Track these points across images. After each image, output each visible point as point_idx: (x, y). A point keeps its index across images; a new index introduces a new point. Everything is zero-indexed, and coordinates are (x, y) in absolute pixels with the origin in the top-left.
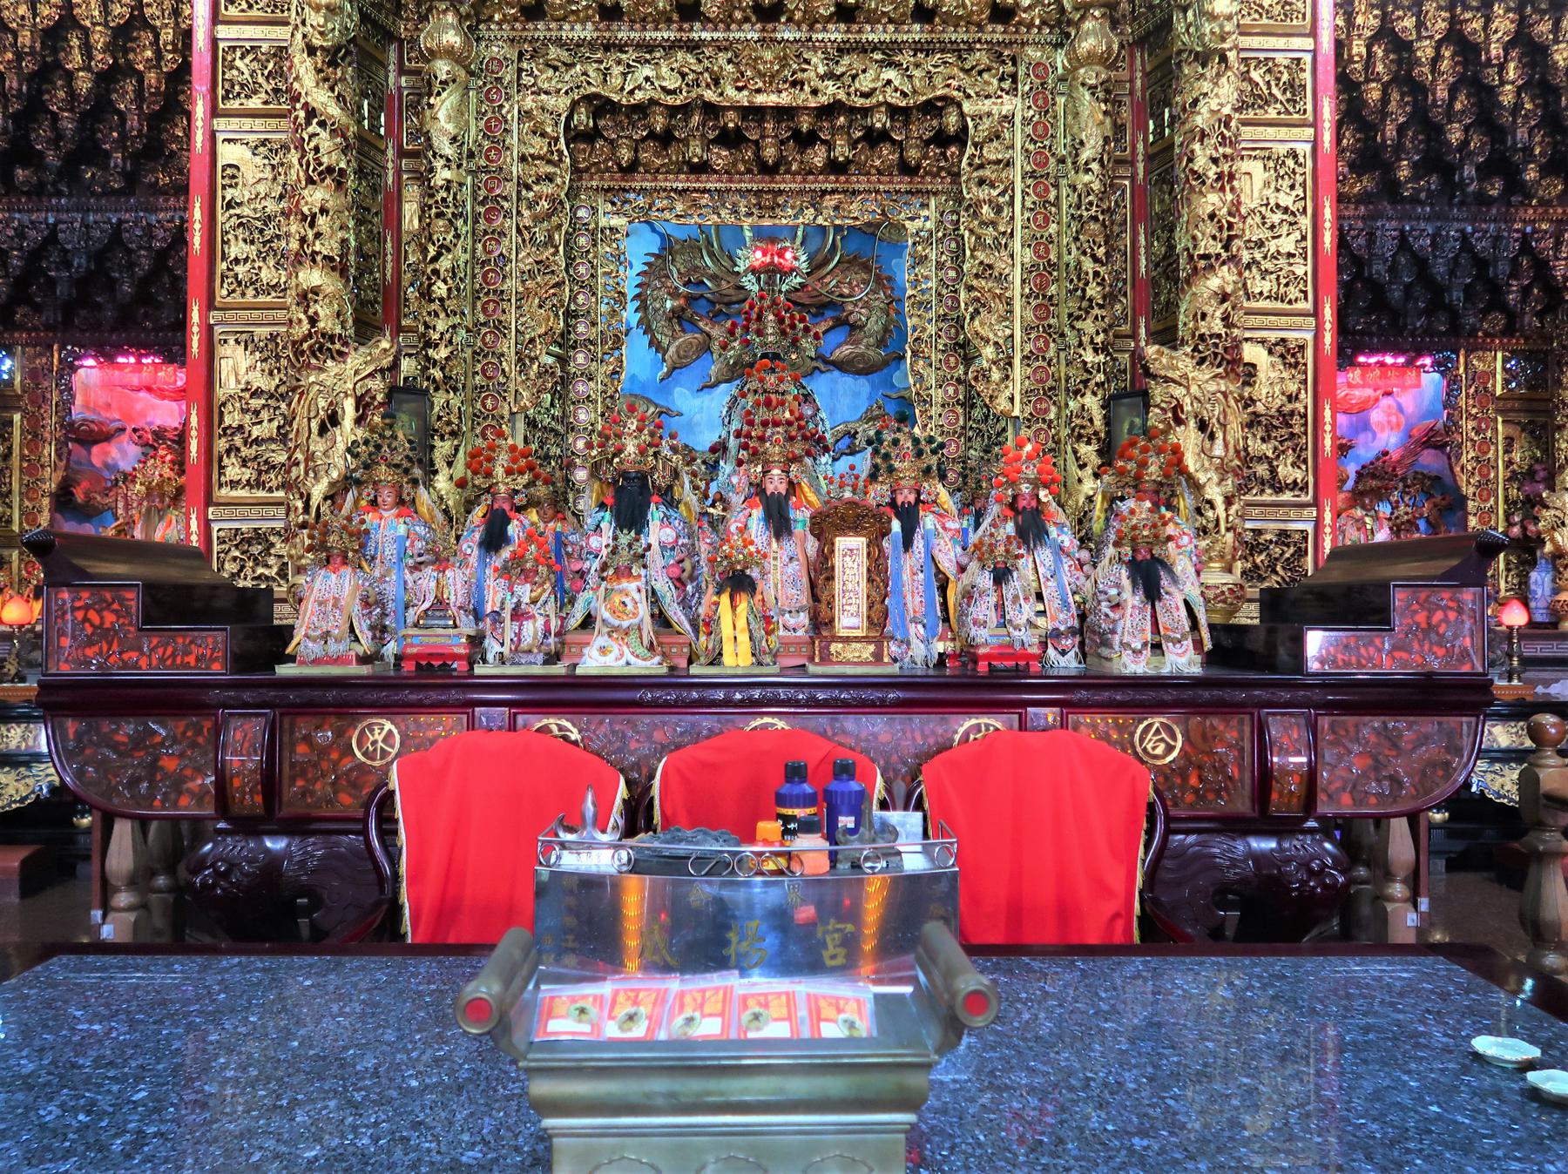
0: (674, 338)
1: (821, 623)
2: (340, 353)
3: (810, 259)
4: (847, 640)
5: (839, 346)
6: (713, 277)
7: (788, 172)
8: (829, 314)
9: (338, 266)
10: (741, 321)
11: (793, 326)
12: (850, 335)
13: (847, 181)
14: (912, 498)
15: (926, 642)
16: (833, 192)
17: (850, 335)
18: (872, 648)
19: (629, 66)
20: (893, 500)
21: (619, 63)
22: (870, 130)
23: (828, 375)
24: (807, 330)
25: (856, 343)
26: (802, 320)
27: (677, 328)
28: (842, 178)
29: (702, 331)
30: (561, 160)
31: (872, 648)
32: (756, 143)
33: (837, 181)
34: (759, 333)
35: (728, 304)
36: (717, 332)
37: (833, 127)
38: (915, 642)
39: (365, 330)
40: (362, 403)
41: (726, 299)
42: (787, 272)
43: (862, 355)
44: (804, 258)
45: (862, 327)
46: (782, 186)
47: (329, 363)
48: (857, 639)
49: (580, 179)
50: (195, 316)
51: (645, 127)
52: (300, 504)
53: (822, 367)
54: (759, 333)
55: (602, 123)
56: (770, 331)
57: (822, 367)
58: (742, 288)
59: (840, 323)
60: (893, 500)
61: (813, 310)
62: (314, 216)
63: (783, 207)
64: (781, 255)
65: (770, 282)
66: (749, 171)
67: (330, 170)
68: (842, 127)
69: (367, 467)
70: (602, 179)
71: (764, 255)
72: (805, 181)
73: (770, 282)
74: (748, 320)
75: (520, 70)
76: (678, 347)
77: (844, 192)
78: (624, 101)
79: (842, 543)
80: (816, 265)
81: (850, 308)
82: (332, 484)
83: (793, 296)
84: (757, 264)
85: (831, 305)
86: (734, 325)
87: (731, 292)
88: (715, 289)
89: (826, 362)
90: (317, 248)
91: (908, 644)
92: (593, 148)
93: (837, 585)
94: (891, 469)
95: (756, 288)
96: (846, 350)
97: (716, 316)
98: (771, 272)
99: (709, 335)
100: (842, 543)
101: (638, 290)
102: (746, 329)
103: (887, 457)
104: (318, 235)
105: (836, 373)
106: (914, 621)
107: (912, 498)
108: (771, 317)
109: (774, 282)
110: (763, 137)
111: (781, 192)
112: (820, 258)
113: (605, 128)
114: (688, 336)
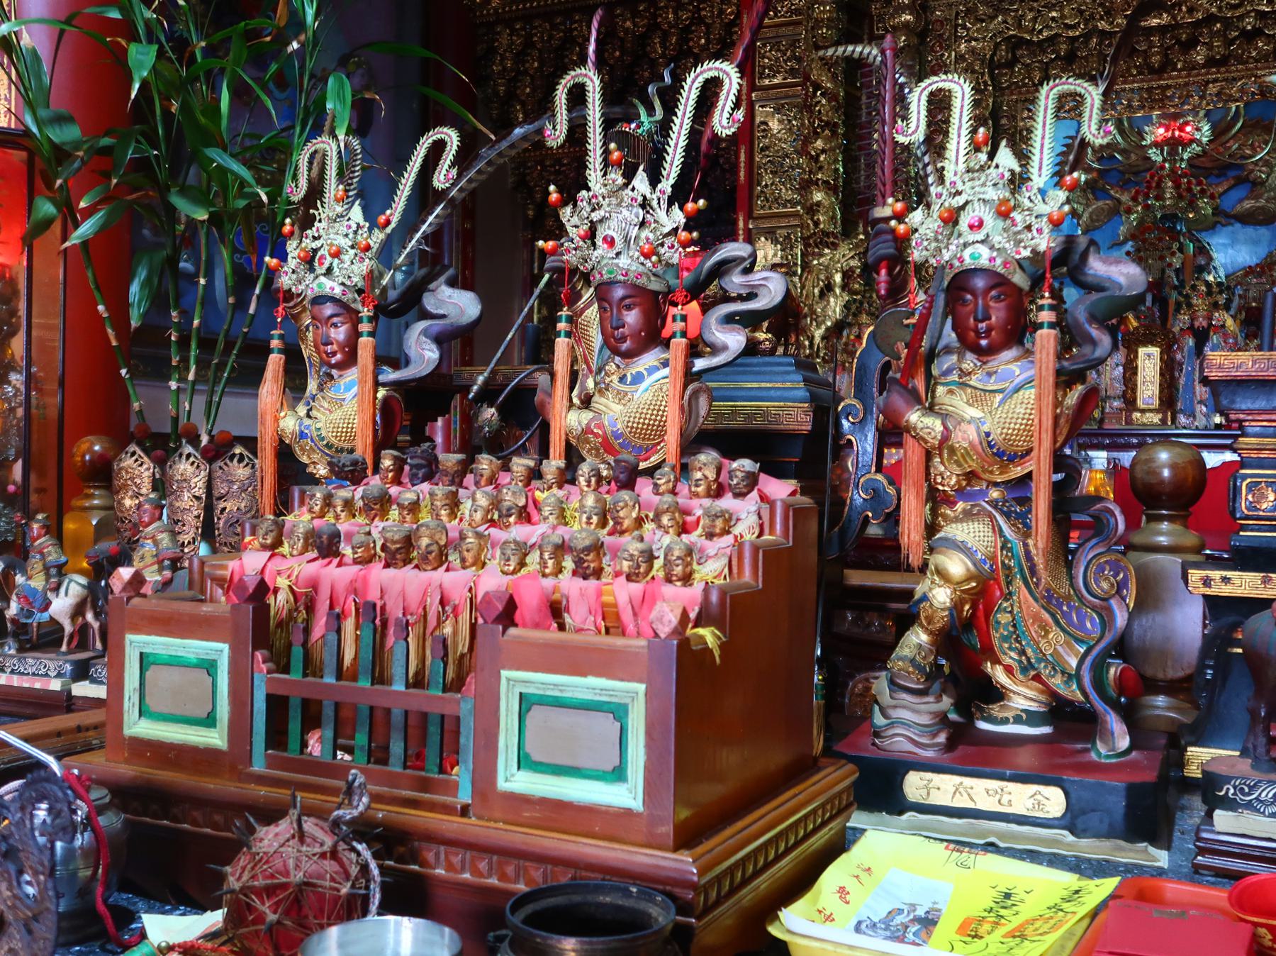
0: (1087, 205)
1: (1130, 401)
2: (833, 244)
3: (1213, 128)
4: (1143, 411)
5: (1241, 201)
6: (1122, 152)
7: (1175, 69)
8: (1232, 173)
9: (829, 188)
10: (1143, 188)
11: (1189, 190)
12: (1252, 191)
13: (1227, 71)
14: (1205, 324)
15: (1207, 416)
16: (1215, 81)
17: (1252, 191)
18: (1160, 416)
19: (1039, 11)
20: (1192, 325)
21: (1031, 10)
22: (1244, 33)
23: (1230, 228)
24: (1203, 192)
25: (1257, 198)
26: (1199, 183)
27: (1090, 196)
28: (1223, 69)
29: (1112, 198)
30: (986, 89)
31: (1160, 416)
32: (1145, 51)
33: (1218, 72)
34: (1159, 198)
35: (1136, 174)
36: (1125, 198)
37: (1211, 31)
38: (1198, 415)
39: (848, 231)
40: (847, 275)
41: (1134, 170)
42: (1186, 144)
43: (1262, 208)
44: (1206, 128)
45: (1263, 183)
46: (1170, 82)
47: (826, 251)
48: (1151, 411)
49: (1003, 95)
50: (741, 224)
51: (1053, 52)
52: (807, 343)
53: (1223, 221)
54: (1159, 198)
55: (1019, 53)
56: (1168, 196)
57: (1223, 221)
58: (1149, 158)
59: (1240, 181)
60: (1192, 325)
61: (1216, 172)
62: (818, 156)
63: (1171, 98)
64: (1181, 129)
65: (1173, 152)
66: (1139, 73)
67: (827, 124)
68: (1219, 31)
69: (855, 315)
70: (1020, 93)
71: (1167, 131)
72: (1189, 76)
73: (1173, 152)
74: (1149, 188)
75: (957, 25)
76: (1091, 214)
77: (1225, 80)
78: (1035, 39)
79: (1142, 351)
80: (1219, 132)
81: (1251, 167)
82: (828, 329)
83: (1196, 162)
84: (1159, 139)
85: (1230, 166)
86: (1137, 192)
87: (1140, 163)
88: (1126, 162)
89: (1228, 216)
90: (819, 176)
91: (1195, 417)
92: (1013, 72)
93: (1139, 379)
94: (1190, 305)
95: (1160, 159)
96: (1248, 204)
97: (1124, 186)
98: (1173, 145)
99: (1119, 201)
100: (1142, 351)
101: (1057, 168)
102: (1147, 197)
103: (1187, 297)
104: (821, 168)
105: (1238, 225)
106: (1200, 402)
107: (1205, 324)
108: (1170, 184)
109: (1177, 153)
110: (1150, 47)
111: (1168, 87)
112: (1223, 125)
113: (1022, 56)
114: (1100, 203)
